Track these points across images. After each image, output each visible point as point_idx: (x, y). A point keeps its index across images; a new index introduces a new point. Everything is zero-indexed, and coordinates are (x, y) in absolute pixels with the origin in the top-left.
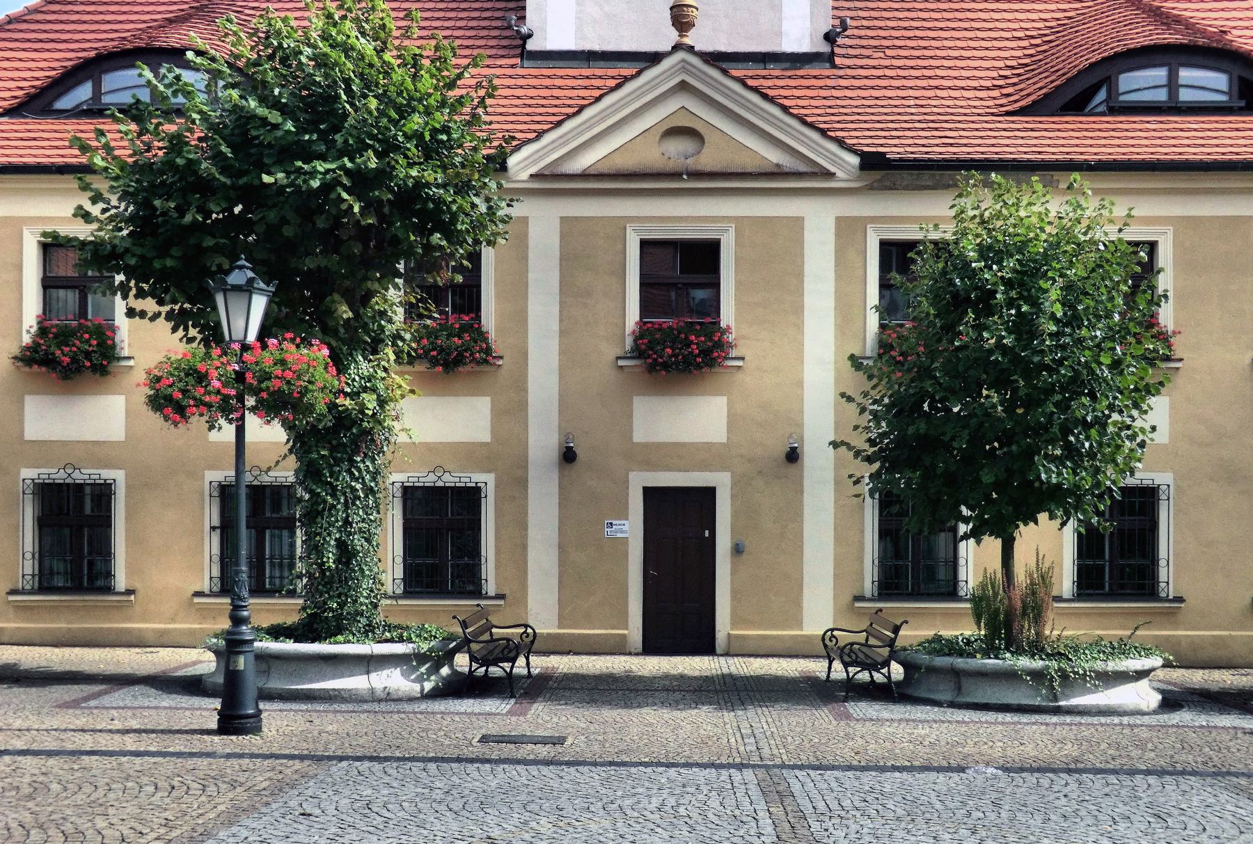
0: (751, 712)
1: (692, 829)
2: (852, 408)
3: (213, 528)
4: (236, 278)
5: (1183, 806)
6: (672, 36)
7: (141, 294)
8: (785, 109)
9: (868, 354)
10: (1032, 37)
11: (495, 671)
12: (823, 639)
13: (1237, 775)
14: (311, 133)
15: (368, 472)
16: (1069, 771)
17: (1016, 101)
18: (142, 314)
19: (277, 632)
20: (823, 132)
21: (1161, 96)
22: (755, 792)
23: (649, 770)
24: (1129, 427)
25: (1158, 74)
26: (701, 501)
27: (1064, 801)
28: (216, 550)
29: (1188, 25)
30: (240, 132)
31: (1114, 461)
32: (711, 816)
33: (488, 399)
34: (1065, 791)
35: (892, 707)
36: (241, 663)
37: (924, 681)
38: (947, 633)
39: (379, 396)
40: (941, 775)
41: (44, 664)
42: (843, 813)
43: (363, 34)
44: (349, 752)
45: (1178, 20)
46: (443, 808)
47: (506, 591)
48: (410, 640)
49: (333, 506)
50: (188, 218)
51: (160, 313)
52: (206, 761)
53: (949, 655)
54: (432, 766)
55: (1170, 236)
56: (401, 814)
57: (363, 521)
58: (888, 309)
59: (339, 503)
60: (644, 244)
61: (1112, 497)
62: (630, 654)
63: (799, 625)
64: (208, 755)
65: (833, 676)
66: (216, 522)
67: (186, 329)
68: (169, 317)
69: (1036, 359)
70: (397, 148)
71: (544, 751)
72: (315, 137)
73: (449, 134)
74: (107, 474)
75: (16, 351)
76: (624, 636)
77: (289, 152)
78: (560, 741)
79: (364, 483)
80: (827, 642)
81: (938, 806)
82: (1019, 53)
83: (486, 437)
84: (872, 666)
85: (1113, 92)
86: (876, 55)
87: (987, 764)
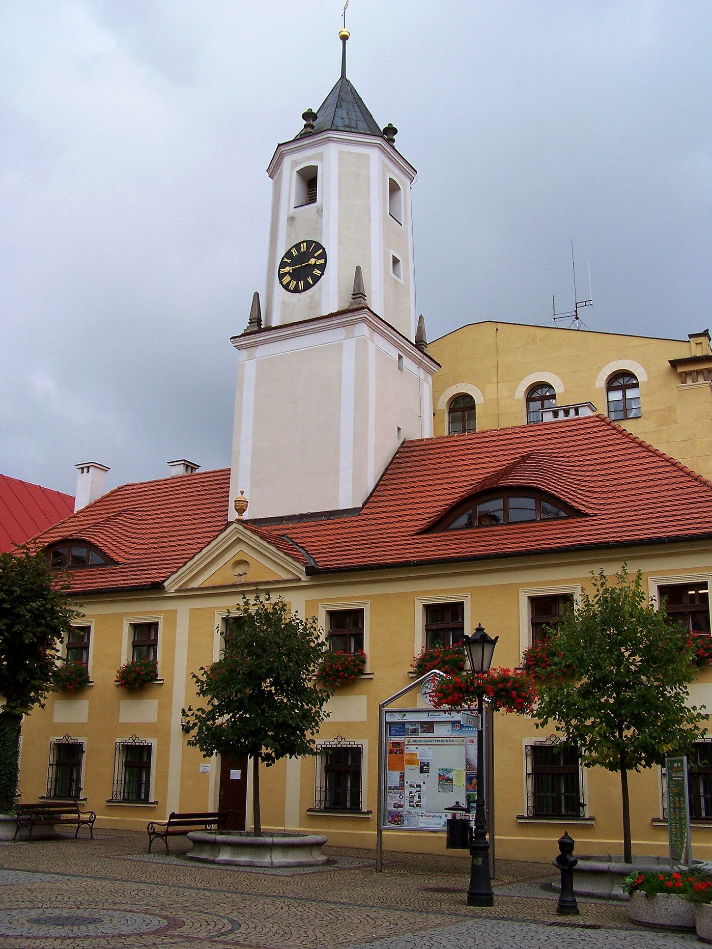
66: (530, 771)
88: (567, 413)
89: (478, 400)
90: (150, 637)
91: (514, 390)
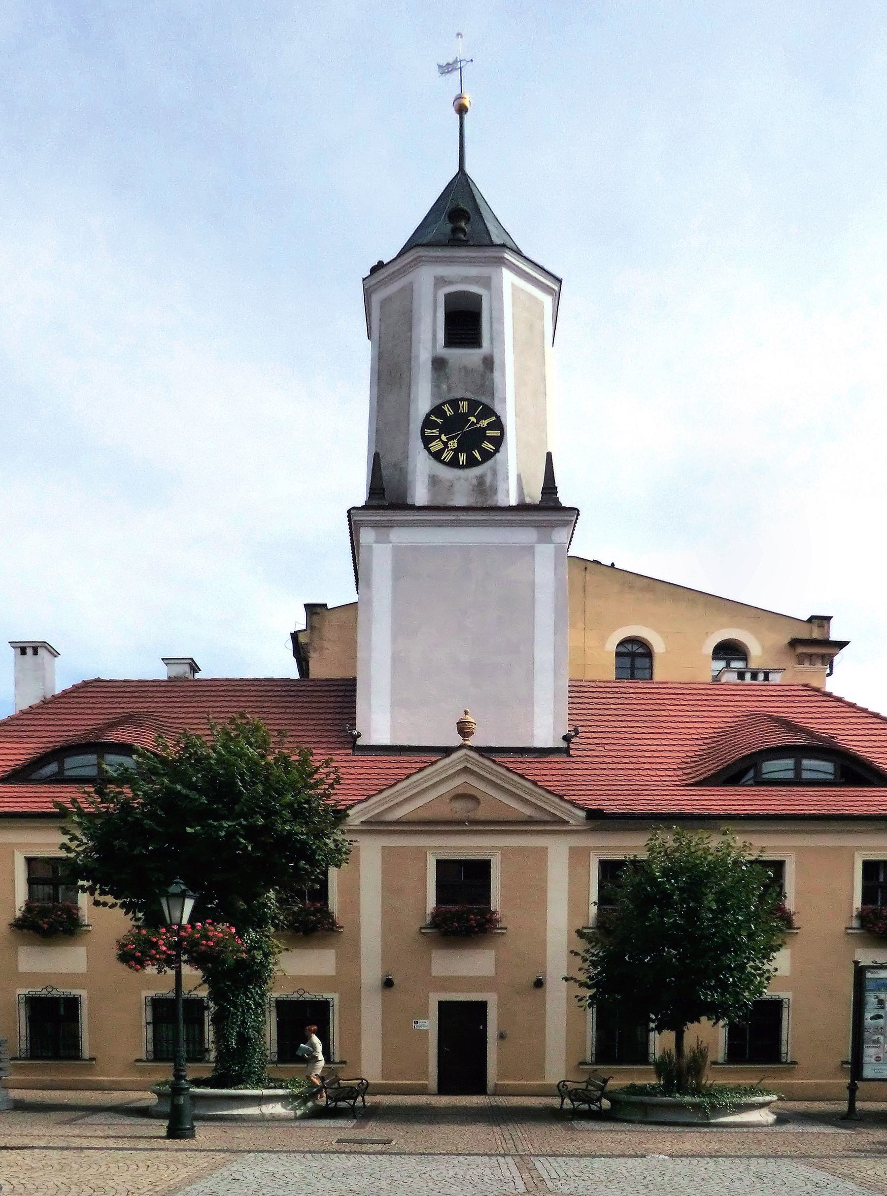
0: (510, 1127)
1: (474, 1186)
2: (578, 959)
3: (148, 1023)
4: (174, 889)
7: (103, 893)
8: (534, 783)
9: (591, 925)
11: (342, 1104)
13: (813, 1157)
14: (218, 804)
15: (257, 993)
16: (711, 1157)
17: (693, 778)
18: (105, 904)
19: (198, 1083)
20: (561, 797)
21: (790, 775)
22: (513, 1168)
23: (446, 1157)
24: (760, 969)
25: (789, 763)
27: (704, 1171)
28: (150, 1035)
29: (810, 733)
30: (169, 805)
31: (749, 989)
32: (486, 1180)
34: (707, 1166)
35: (604, 1124)
36: (182, 1101)
37: (626, 1110)
38: (639, 1082)
39: (264, 952)
40: (630, 1160)
41: (39, 1100)
42: (567, 1179)
43: (251, 745)
44: (253, 1148)
45: (803, 730)
46: (320, 1176)
47: (345, 1059)
48: (288, 1088)
49: (235, 1013)
50: (136, 852)
51: (116, 904)
52: (163, 1153)
53: (640, 1095)
54: (309, 1156)
55: (794, 858)
56: (295, 1179)
57: (255, 1021)
58: (604, 900)
59: (238, 1011)
60: (439, 863)
61: (747, 1008)
62: (430, 1094)
64: (164, 1150)
65: (565, 1106)
66: (150, 1019)
67: (134, 913)
68: (123, 906)
69: (699, 932)
70: (276, 813)
71: (378, 1147)
72: (220, 806)
73: (309, 804)
74: (75, 992)
75: (12, 921)
76: (426, 1085)
77: (201, 815)
79: (255, 1000)
81: (626, 1174)
82: (696, 748)
84: (590, 1101)
85: (758, 773)
86: (598, 749)
87: (660, 1153)
88: (754, 676)
89: (658, 646)
90: (878, 879)
91: (603, 640)
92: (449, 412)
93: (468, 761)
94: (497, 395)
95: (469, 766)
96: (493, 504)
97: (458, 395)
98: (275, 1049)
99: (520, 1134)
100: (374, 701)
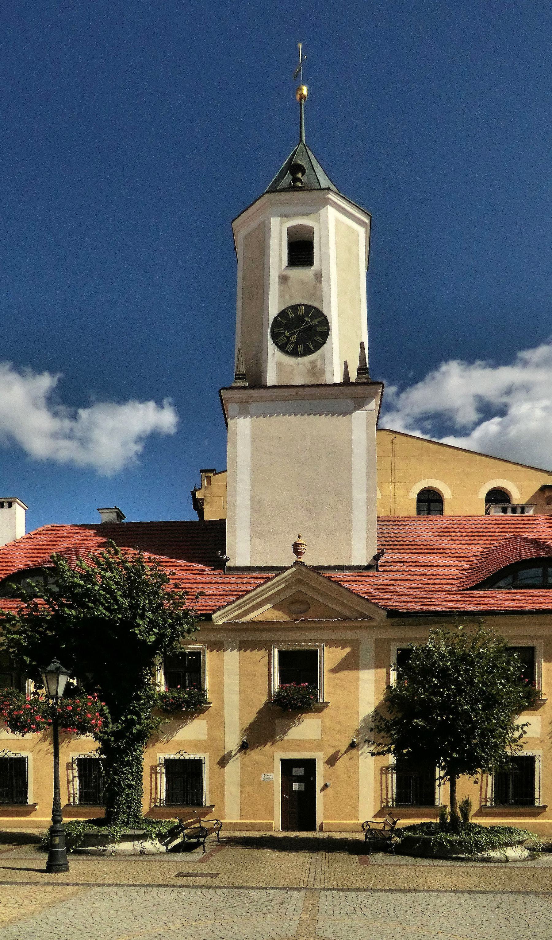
4: (52, 667)
5: (522, 913)
6: (294, 558)
10: (477, 556)
12: (363, 826)
26: (309, 765)
33: (205, 721)
37: (416, 846)
63: (357, 819)
71: (205, 881)
78: (215, 875)
80: (365, 827)
83: (205, 738)
89: (447, 493)
91: (408, 491)
92: (292, 315)
93: (302, 574)
94: (325, 301)
95: (301, 578)
96: (323, 382)
97: (297, 302)
98: (164, 795)
99: (323, 868)
100: (238, 532)
